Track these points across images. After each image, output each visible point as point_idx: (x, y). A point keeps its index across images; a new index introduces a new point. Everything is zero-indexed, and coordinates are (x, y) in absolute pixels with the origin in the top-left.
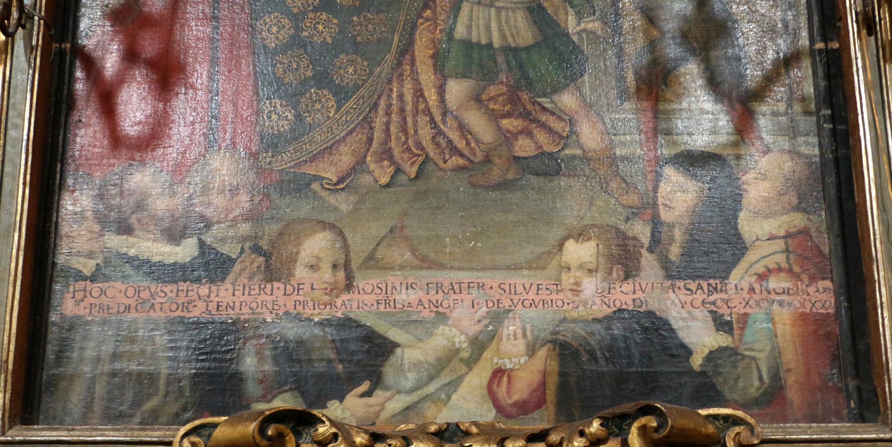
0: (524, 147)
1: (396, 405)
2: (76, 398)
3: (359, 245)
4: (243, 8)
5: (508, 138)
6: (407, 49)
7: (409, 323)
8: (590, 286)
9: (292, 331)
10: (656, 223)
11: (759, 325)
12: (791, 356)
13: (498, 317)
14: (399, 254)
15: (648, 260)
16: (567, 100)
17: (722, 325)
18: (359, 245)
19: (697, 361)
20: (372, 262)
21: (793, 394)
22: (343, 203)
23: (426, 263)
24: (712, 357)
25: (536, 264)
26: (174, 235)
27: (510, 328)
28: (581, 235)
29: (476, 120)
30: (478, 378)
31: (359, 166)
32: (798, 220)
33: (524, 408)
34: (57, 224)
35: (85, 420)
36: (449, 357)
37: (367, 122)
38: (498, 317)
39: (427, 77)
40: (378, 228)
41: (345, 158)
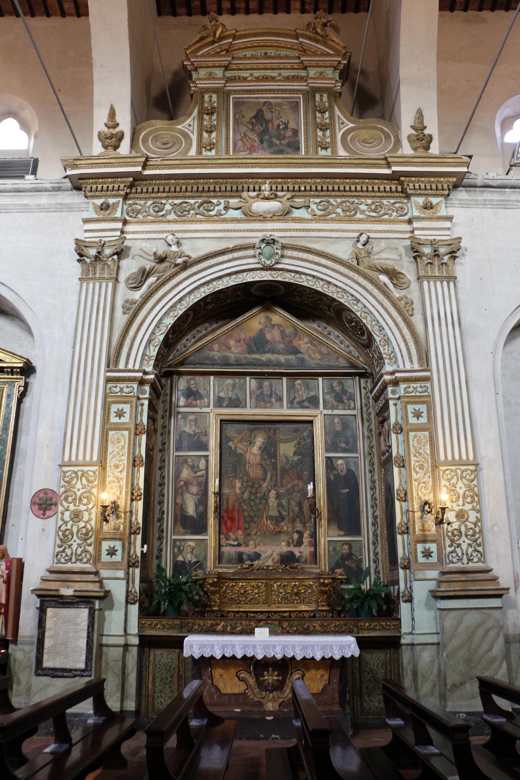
0: (277, 530)
1: (261, 562)
2: (224, 560)
3: (257, 543)
4: (248, 481)
5: (275, 529)
6: (262, 516)
7: (263, 552)
8: (284, 548)
9: (249, 553)
10: (293, 540)
11: (305, 553)
12: (308, 556)
13: (273, 552)
14: (262, 544)
15: (292, 545)
16: (282, 524)
17: (300, 553)
18: (257, 543)
19: (355, 569)
20: (258, 545)
21: (308, 561)
22: (255, 537)
23: (265, 545)
24: (299, 557)
25: (278, 545)
26: (234, 541)
27: (275, 553)
28: (283, 541)
29: (271, 526)
30: (271, 559)
31: (257, 532)
32: (310, 539)
33: (276, 563)
34: (436, 624)
35: (225, 563)
36: (267, 557)
37: (258, 526)
38: (273, 552)
39: (265, 520)
40: (259, 540)
41: (255, 531)
